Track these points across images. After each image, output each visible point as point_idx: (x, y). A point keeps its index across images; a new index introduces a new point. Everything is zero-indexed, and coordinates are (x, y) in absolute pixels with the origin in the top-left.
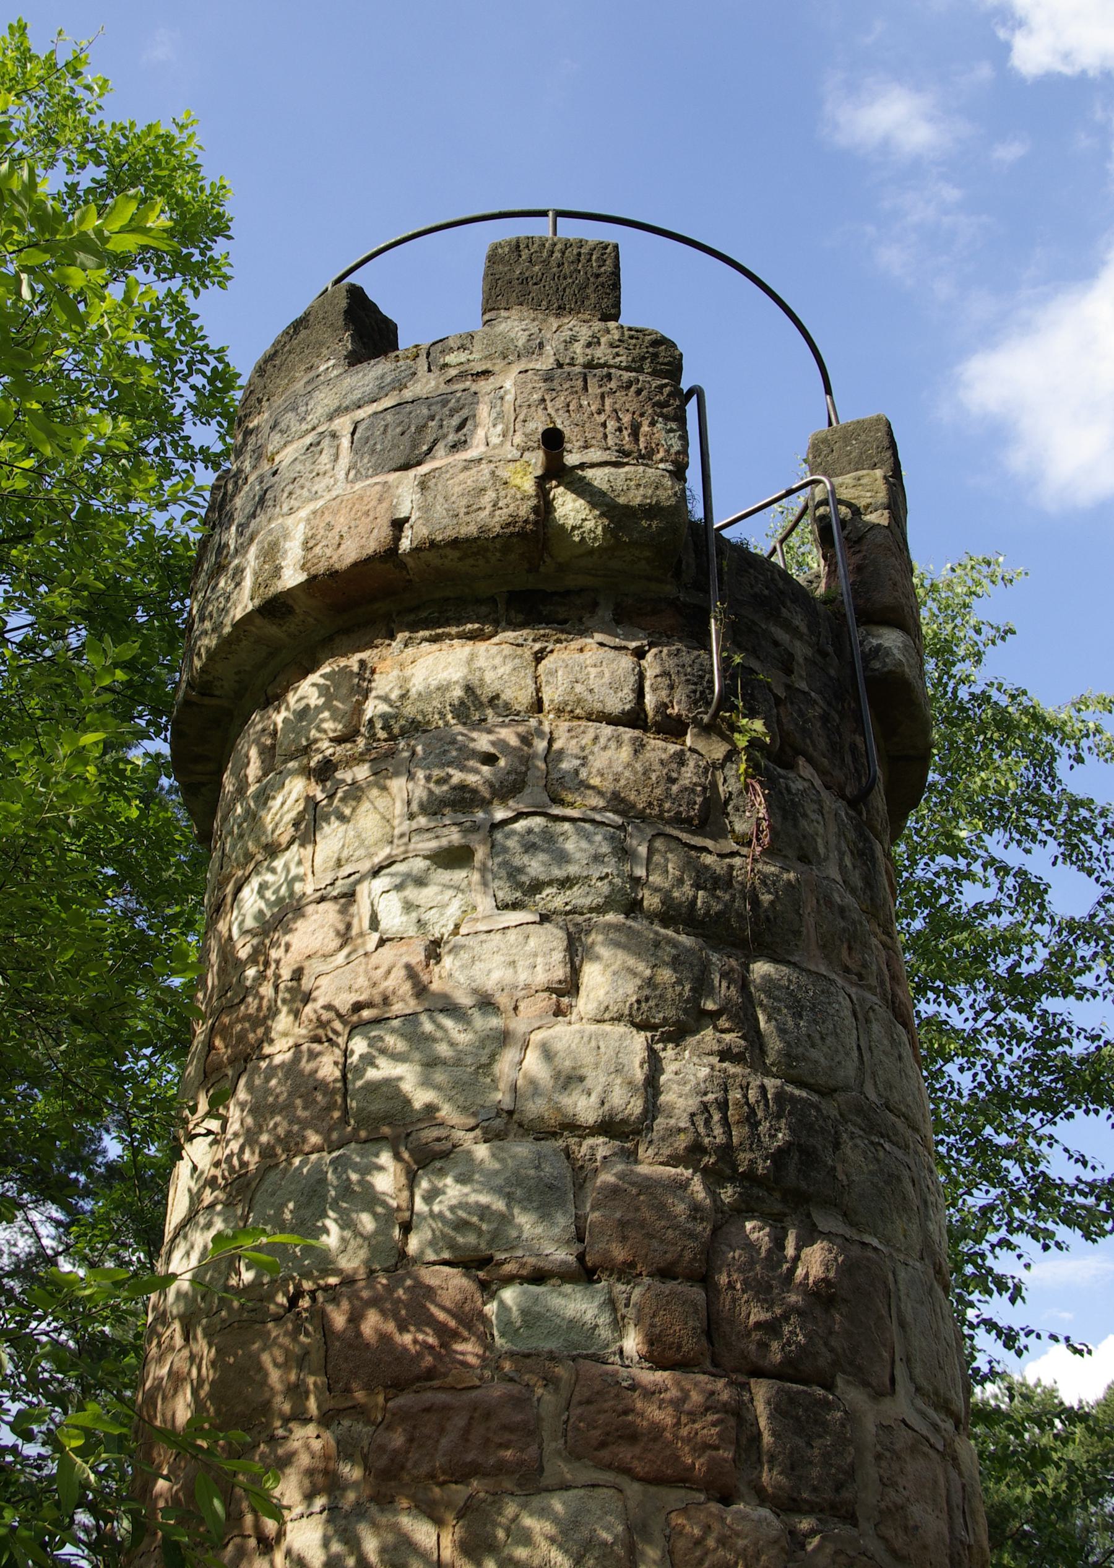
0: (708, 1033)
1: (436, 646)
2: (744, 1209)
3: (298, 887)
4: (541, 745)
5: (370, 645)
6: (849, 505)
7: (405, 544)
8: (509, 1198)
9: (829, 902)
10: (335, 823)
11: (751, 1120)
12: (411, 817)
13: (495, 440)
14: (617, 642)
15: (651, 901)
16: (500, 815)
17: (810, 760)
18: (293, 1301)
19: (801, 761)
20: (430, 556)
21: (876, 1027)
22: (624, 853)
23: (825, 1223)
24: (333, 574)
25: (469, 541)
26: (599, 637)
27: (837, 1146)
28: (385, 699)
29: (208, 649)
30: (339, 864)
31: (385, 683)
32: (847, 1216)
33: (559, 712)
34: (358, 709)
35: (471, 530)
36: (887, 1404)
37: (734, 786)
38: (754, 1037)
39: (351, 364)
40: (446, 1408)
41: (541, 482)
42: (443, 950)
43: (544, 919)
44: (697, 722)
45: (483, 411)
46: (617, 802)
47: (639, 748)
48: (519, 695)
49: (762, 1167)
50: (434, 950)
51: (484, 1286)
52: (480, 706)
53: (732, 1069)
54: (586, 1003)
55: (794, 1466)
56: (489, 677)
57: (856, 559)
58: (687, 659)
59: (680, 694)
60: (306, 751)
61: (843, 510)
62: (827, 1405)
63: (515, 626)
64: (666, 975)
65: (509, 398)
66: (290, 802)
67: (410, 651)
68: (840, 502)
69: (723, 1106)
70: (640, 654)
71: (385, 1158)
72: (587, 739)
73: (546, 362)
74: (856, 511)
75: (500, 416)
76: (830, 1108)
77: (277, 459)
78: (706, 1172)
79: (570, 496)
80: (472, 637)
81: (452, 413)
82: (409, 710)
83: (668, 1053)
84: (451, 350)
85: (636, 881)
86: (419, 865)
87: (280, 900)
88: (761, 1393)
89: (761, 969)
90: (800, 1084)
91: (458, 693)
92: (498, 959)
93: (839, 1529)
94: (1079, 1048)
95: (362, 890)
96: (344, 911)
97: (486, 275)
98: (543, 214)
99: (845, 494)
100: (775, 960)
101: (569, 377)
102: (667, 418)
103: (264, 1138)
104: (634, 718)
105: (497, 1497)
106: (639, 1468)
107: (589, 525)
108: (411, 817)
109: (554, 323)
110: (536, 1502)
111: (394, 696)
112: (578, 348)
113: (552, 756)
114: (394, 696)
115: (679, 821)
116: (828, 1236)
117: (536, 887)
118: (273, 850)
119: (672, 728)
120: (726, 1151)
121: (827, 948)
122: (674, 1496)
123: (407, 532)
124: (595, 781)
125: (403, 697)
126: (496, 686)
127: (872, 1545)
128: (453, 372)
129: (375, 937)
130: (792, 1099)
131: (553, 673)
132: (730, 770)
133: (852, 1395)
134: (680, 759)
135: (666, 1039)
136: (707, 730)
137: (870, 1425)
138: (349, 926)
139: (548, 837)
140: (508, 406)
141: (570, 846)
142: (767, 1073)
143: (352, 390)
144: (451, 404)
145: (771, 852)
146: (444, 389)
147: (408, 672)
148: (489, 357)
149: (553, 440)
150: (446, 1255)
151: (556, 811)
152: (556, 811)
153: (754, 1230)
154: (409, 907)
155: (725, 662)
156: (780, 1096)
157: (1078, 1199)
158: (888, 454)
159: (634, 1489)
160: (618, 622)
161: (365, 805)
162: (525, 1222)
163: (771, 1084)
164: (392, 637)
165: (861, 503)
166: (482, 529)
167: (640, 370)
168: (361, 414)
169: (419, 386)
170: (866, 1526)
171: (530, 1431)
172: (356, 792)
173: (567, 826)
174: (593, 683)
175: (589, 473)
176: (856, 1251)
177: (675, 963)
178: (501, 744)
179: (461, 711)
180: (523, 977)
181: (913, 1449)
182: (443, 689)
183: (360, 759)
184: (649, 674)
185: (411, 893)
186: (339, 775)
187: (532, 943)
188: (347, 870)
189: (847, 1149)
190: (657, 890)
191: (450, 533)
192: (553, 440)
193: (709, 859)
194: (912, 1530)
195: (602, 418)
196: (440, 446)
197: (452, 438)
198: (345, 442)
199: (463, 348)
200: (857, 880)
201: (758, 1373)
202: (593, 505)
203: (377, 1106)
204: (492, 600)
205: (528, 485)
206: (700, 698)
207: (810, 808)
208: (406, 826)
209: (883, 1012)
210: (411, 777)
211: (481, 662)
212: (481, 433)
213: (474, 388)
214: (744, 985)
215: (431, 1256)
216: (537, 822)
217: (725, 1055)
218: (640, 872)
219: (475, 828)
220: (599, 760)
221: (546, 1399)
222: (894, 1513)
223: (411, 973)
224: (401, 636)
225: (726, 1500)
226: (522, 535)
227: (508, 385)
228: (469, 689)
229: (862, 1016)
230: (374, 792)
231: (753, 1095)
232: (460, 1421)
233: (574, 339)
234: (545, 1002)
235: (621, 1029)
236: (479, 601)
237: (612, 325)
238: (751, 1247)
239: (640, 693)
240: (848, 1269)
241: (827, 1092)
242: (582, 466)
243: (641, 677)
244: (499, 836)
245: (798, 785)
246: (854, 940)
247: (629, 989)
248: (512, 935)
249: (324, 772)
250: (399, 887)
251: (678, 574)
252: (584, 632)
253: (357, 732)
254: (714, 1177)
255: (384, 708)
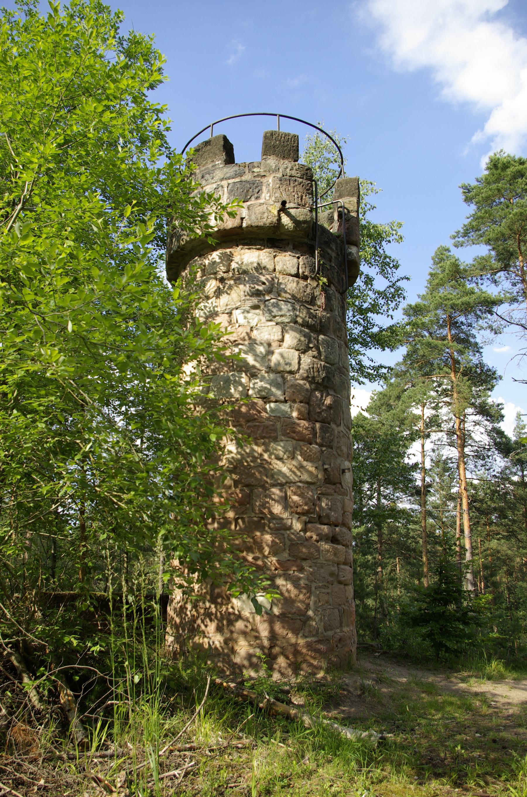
0: (310, 352)
1: (249, 251)
2: (316, 389)
3: (216, 309)
4: (276, 281)
5: (231, 248)
6: (347, 209)
7: (244, 225)
8: (271, 385)
9: (336, 321)
10: (226, 295)
11: (318, 371)
12: (245, 296)
13: (268, 198)
14: (294, 254)
15: (300, 320)
16: (267, 298)
17: (334, 285)
18: (223, 403)
19: (332, 285)
20: (251, 229)
21: (343, 349)
22: (294, 309)
23: (331, 392)
24: (225, 230)
25: (260, 226)
26: (289, 253)
27: (334, 376)
28: (237, 263)
29: (186, 240)
30: (227, 305)
31: (237, 258)
32: (335, 391)
33: (280, 272)
34: (229, 265)
35: (261, 224)
36: (339, 428)
37: (318, 293)
38: (320, 353)
39: (226, 164)
40: (258, 426)
41: (279, 211)
42: (254, 329)
43: (277, 324)
44: (311, 277)
45: (264, 188)
46: (294, 297)
47: (298, 283)
48: (271, 267)
49: (320, 381)
50: (252, 329)
51: (265, 403)
52: (261, 269)
53: (315, 360)
54: (286, 344)
55: (323, 439)
56: (263, 262)
57: (347, 225)
58: (309, 260)
59: (307, 269)
60: (215, 273)
61: (345, 210)
62: (329, 428)
63: (269, 248)
64: (303, 339)
65: (271, 185)
66: (212, 286)
67: (243, 251)
68: (345, 208)
69: (313, 368)
70: (298, 258)
71: (244, 375)
72: (286, 280)
73: (279, 175)
74: (349, 212)
75: (269, 191)
76: (333, 368)
77: (204, 188)
78: (309, 382)
79: (286, 216)
80: (258, 249)
81: (257, 187)
82: (244, 268)
83: (302, 356)
84: (255, 167)
85: (297, 316)
86: (248, 308)
87: (211, 311)
88: (318, 425)
89: (321, 337)
90: (328, 363)
91: (255, 265)
92: (267, 333)
93: (330, 450)
94: (375, 330)
95: (234, 312)
96: (230, 316)
97: (263, 144)
98: (276, 115)
99: (346, 206)
100: (324, 335)
101: (286, 180)
102: (309, 194)
103: (212, 367)
104: (297, 275)
105: (270, 442)
106: (297, 438)
107: (290, 225)
108: (245, 296)
109: (282, 161)
110: (277, 443)
111: (240, 263)
112: (288, 170)
113: (279, 284)
114: (240, 263)
115: (306, 302)
116: (331, 395)
117: (275, 317)
118: (208, 298)
119: (305, 278)
120: (313, 378)
121: (335, 332)
122: (301, 443)
123: (244, 221)
124: (289, 291)
125: (242, 263)
126: (265, 264)
127: (335, 453)
128: (256, 174)
129: (237, 325)
130: (326, 367)
131: (278, 262)
132: (317, 289)
133: (333, 426)
134: (307, 286)
135: (302, 353)
136: (313, 279)
137: (336, 432)
138: (231, 321)
139: (277, 304)
140: (271, 188)
141: (283, 307)
142: (322, 361)
143: (227, 173)
144: (256, 185)
145: (325, 310)
146: (253, 179)
147: (243, 257)
148: (265, 171)
149: (284, 203)
150: (258, 396)
151: (280, 298)
152: (280, 298)
153: (318, 394)
154: (245, 318)
155: (319, 262)
156: (324, 366)
157: (369, 371)
158: (357, 191)
159: (294, 442)
160: (294, 249)
161: (233, 292)
162: (274, 390)
163: (323, 363)
164: (238, 246)
165: (350, 209)
166: (265, 224)
167: (303, 178)
168: (230, 181)
169: (246, 177)
170: (334, 450)
171: (275, 430)
172: (230, 287)
173: (282, 302)
174: (288, 265)
175: (290, 210)
176: (336, 398)
177: (305, 336)
178: (267, 279)
179: (256, 269)
180: (272, 338)
181: (343, 436)
182: (252, 263)
183: (231, 278)
184: (301, 264)
185: (246, 314)
186: (226, 282)
187: (274, 330)
188: (229, 307)
189: (336, 377)
190: (302, 318)
191: (256, 224)
192: (284, 203)
193: (312, 311)
194: (342, 451)
195: (294, 194)
196: (253, 197)
197: (256, 195)
198: (226, 189)
199: (258, 167)
200: (341, 314)
201: (317, 421)
202: (291, 220)
203: (241, 364)
204: (263, 240)
205: (276, 213)
206: (312, 271)
207: (333, 298)
208: (244, 298)
209: (344, 345)
210: (245, 285)
211: (261, 257)
212: (263, 195)
213: (261, 180)
214: (318, 341)
215: (255, 396)
216: (274, 300)
217: (314, 357)
218: (298, 313)
219: (261, 301)
220: (289, 286)
221: (279, 425)
222: (339, 448)
223: (247, 333)
224: (240, 247)
225: (311, 444)
226: (274, 227)
227: (270, 181)
228: (258, 264)
229: (340, 347)
230: (235, 288)
231: (319, 366)
232: (262, 428)
233: (287, 168)
234: (277, 343)
235: (293, 351)
236: (260, 240)
237: (296, 163)
238: (317, 397)
239: (298, 269)
240: (334, 402)
241: (332, 365)
242: (289, 208)
243: (299, 264)
244: (267, 303)
245: (331, 292)
246: (340, 330)
247: (295, 342)
248: (270, 328)
249: (222, 280)
250: (243, 313)
251: (308, 236)
252: (285, 251)
253: (229, 271)
254: (310, 383)
255: (237, 266)
